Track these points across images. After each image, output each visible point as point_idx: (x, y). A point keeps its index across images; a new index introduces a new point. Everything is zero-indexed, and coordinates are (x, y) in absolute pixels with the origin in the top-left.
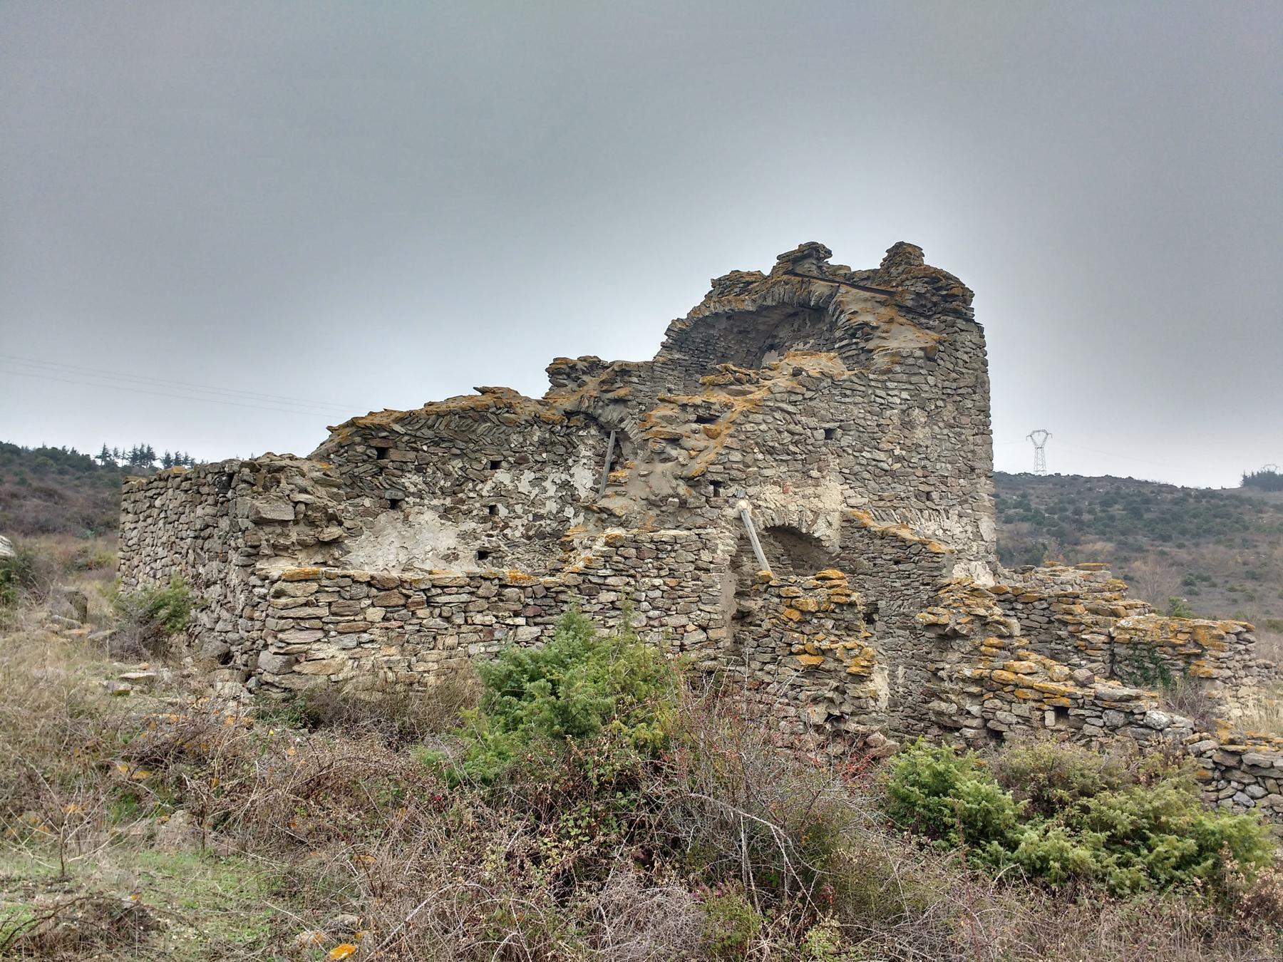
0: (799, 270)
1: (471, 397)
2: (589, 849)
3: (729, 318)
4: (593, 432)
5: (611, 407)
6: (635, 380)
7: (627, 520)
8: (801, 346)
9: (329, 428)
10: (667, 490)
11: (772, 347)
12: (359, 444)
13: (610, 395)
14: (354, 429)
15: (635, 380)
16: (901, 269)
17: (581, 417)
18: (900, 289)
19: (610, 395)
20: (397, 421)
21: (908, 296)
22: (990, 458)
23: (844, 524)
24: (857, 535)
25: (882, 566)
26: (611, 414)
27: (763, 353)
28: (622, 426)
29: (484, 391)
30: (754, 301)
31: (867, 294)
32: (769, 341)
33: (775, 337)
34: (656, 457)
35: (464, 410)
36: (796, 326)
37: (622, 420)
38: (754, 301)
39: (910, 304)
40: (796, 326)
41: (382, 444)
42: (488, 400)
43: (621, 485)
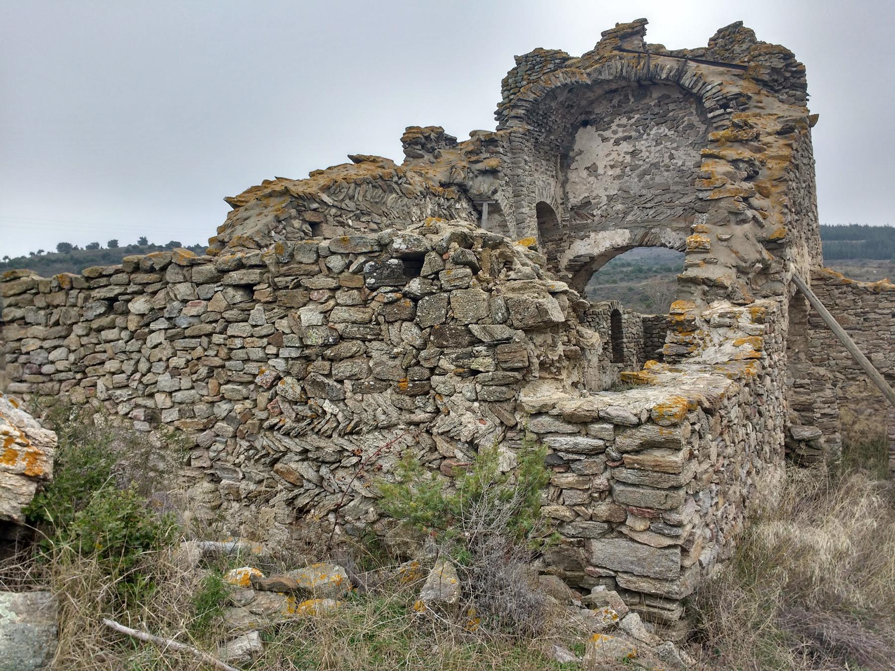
0: (626, 46)
1: (345, 166)
2: (251, 593)
3: (570, 91)
4: (465, 205)
5: (480, 178)
6: (501, 150)
7: (733, 292)
8: (624, 121)
9: (229, 200)
10: (753, 256)
11: (585, 124)
12: (295, 218)
13: (480, 166)
14: (288, 199)
15: (501, 150)
16: (745, 46)
17: (454, 188)
18: (752, 64)
19: (480, 166)
20: (326, 189)
21: (763, 71)
22: (816, 219)
23: (815, 283)
24: (836, 292)
25: (876, 320)
26: (482, 185)
27: (575, 129)
28: (496, 197)
29: (358, 160)
30: (589, 74)
31: (721, 69)
32: (583, 117)
33: (590, 113)
34: (732, 218)
35: (375, 178)
36: (615, 102)
37: (495, 192)
38: (589, 74)
39: (766, 78)
40: (615, 102)
41: (314, 219)
42: (365, 171)
43: (706, 251)
